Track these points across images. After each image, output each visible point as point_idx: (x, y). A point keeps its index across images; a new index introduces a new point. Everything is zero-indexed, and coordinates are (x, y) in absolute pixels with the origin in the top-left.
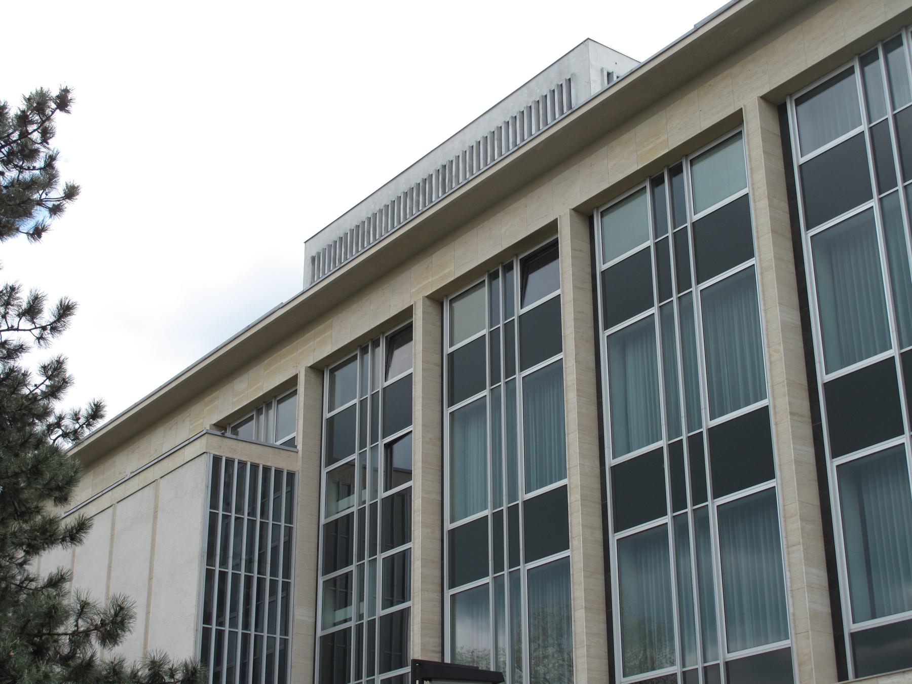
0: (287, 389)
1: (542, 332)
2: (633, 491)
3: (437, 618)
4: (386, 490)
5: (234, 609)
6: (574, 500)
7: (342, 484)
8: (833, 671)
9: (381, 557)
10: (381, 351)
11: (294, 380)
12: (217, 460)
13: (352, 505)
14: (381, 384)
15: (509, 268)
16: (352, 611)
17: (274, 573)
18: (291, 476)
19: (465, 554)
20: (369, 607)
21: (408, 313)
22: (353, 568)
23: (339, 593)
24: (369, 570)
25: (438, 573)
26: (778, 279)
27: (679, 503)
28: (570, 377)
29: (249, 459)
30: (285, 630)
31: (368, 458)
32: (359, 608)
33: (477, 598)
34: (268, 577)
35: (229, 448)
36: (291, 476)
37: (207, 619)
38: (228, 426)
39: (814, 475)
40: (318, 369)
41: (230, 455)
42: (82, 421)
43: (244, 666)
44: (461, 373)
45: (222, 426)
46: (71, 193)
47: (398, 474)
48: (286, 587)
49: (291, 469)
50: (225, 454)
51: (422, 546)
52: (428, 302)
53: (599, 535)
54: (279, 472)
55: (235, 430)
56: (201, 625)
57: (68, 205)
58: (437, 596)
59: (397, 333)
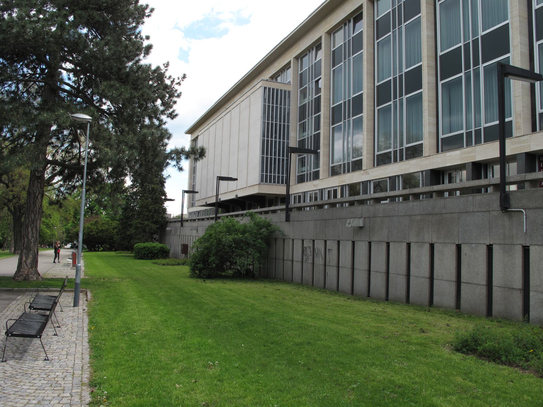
0: (287, 66)
1: (357, 43)
2: (383, 93)
3: (328, 135)
4: (316, 95)
5: (276, 133)
6: (365, 97)
7: (304, 94)
8: (435, 150)
9: (314, 116)
10: (314, 52)
11: (290, 62)
12: (265, 88)
13: (306, 101)
14: (314, 62)
15: (350, 22)
16: (306, 134)
17: (284, 122)
18: (289, 92)
19: (336, 114)
20: (310, 132)
21: (320, 39)
22: (306, 120)
23: (303, 128)
24: (310, 121)
25: (328, 121)
26: (427, 20)
27: (395, 97)
28: (365, 57)
29: (275, 88)
30: (288, 139)
31: (310, 85)
32: (308, 133)
33: (339, 128)
34: (282, 123)
35: (273, 85)
36: (289, 92)
37: (264, 136)
38: (274, 77)
39: (435, 87)
40: (297, 58)
41: (270, 87)
42: (180, 79)
43: (279, 150)
44: (335, 58)
45: (272, 77)
46: (152, 10)
47: (318, 90)
48: (288, 126)
49: (289, 90)
50: (268, 86)
51: (324, 112)
52: (326, 34)
53: (372, 108)
54: (285, 91)
55: (276, 79)
56: (262, 138)
57: (152, 14)
58: (328, 128)
59: (317, 46)
